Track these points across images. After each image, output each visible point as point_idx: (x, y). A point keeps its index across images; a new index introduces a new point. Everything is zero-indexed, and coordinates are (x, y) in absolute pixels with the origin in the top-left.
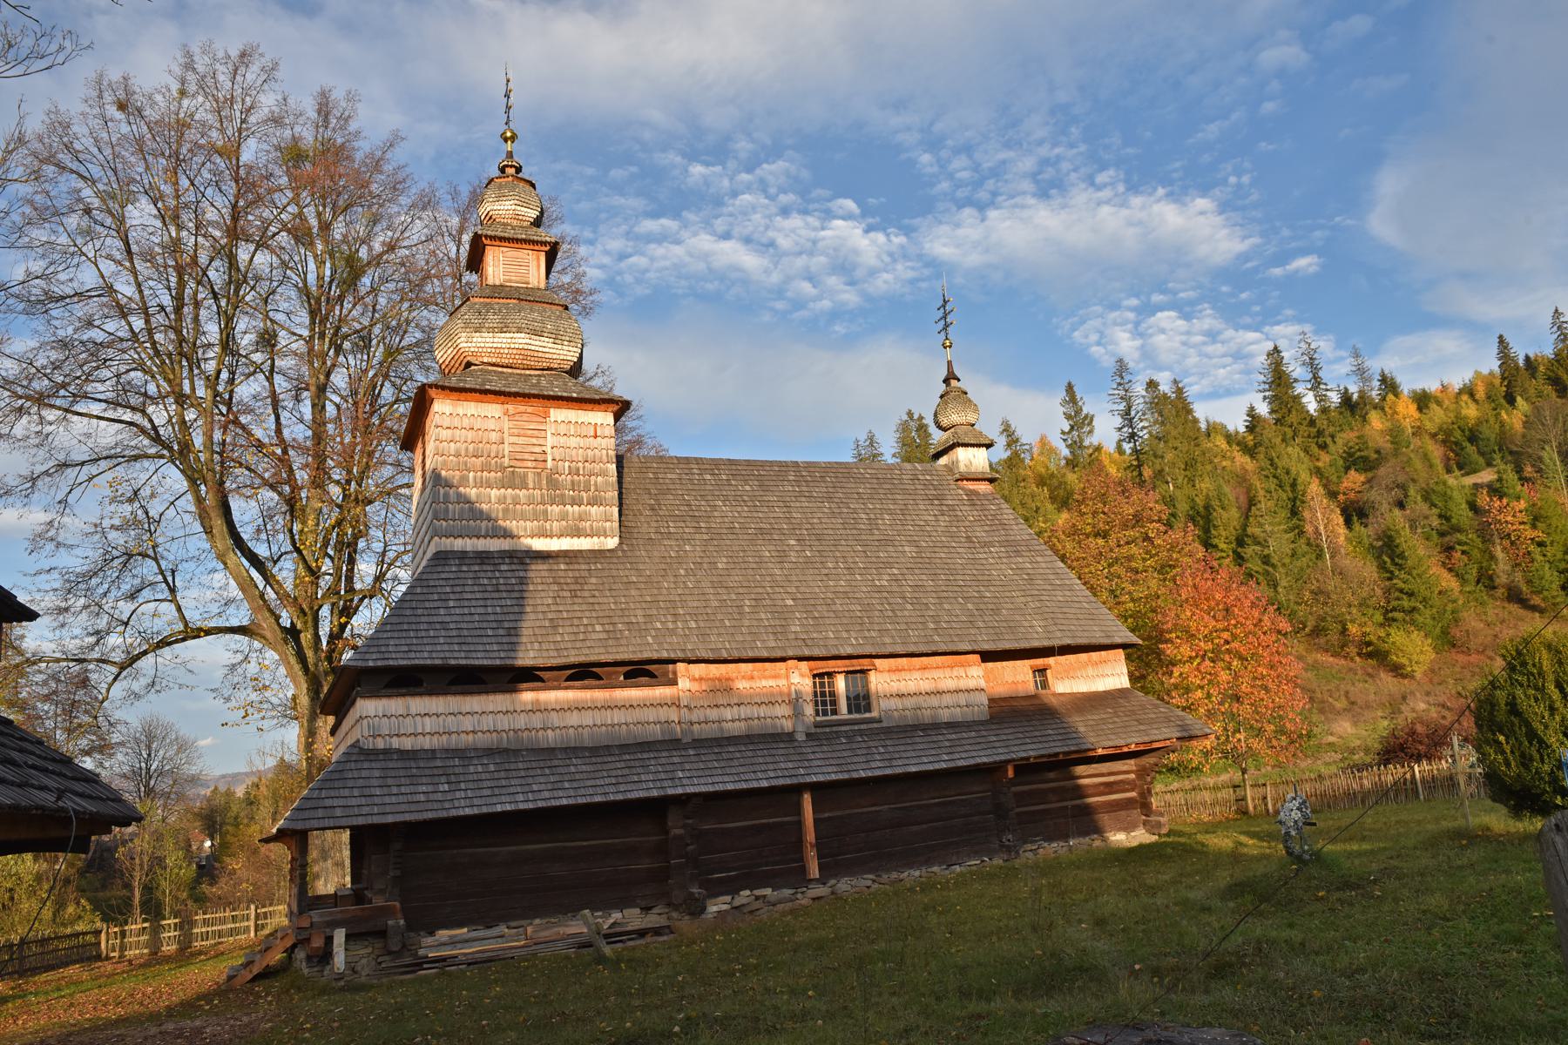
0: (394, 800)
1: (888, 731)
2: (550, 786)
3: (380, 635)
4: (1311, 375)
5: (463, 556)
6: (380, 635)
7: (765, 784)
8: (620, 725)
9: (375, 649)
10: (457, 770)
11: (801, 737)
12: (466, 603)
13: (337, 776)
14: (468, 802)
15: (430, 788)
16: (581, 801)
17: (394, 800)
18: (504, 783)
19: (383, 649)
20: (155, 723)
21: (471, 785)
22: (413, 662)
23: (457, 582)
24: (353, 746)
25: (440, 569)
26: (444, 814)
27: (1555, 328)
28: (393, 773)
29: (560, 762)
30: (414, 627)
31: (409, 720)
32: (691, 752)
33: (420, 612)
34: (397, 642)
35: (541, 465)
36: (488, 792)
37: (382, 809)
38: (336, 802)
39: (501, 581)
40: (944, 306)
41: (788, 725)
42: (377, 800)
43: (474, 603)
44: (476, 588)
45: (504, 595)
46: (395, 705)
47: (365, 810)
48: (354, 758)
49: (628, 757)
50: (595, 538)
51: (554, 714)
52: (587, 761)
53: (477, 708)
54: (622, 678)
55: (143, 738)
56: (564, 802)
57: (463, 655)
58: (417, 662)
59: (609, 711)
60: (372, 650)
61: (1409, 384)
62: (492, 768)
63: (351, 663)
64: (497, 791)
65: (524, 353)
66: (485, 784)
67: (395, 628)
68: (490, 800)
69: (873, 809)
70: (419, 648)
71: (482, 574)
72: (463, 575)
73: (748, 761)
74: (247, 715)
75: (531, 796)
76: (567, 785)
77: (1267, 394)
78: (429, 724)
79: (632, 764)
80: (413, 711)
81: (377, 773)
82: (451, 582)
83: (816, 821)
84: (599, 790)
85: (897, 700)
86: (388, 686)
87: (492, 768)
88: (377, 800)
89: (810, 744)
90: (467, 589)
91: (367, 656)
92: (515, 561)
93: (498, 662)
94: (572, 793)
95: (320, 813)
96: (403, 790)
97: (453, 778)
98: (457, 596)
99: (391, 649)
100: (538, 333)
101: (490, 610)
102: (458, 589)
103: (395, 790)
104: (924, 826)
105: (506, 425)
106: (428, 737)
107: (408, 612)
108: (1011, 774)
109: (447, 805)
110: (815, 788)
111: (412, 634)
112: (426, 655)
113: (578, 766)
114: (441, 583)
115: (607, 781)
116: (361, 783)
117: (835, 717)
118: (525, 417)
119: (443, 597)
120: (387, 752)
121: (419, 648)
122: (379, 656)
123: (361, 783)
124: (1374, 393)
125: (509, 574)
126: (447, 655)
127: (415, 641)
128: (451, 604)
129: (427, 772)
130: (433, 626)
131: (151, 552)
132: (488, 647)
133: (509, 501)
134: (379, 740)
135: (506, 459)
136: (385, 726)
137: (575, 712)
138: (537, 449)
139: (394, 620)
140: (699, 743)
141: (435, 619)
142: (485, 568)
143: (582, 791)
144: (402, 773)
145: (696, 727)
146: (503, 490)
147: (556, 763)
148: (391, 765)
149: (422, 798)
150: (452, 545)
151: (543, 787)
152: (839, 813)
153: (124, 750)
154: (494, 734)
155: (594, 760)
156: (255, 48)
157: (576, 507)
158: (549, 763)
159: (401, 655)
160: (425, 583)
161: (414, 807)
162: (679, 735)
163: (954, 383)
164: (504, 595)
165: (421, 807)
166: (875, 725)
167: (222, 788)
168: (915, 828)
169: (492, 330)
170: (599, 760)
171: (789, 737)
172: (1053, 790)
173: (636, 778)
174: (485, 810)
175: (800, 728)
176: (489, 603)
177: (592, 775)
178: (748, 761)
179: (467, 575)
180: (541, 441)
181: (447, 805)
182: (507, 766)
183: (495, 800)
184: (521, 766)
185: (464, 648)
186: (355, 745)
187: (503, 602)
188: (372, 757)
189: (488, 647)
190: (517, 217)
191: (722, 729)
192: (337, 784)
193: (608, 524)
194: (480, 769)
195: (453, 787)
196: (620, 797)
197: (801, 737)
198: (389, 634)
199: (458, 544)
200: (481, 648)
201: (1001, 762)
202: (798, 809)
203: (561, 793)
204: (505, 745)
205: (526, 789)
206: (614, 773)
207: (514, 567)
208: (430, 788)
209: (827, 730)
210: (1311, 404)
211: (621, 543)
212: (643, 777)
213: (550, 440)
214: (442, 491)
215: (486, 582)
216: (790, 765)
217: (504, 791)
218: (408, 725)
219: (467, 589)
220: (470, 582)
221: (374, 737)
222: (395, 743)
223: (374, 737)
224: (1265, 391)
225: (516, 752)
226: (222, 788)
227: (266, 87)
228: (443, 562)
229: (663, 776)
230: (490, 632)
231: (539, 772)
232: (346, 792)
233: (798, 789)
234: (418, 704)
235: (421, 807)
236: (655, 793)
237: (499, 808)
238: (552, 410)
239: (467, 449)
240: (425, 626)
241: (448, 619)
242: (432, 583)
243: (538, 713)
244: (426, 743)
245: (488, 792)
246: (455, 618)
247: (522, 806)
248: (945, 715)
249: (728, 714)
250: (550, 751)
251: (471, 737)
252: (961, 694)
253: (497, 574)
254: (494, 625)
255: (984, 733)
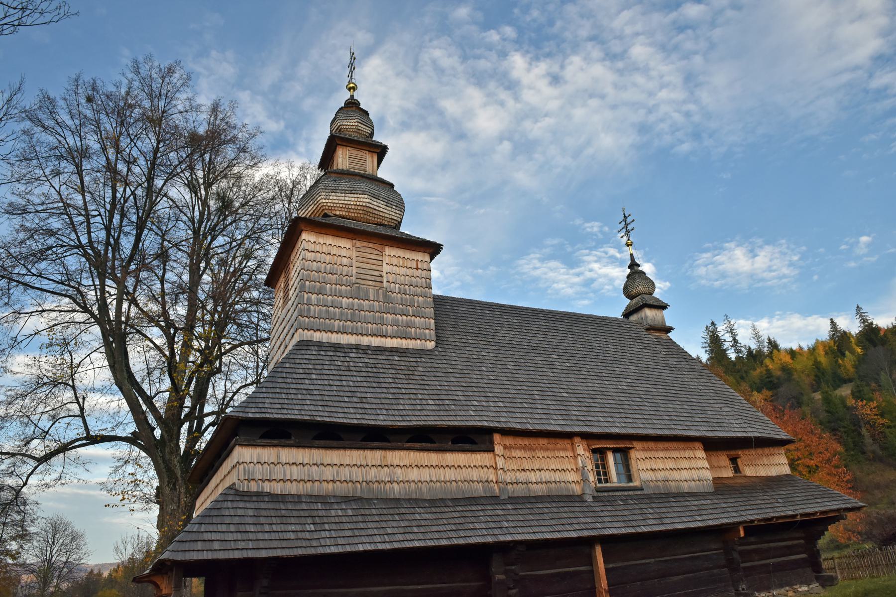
0: (267, 536)
1: (649, 497)
2: (401, 530)
3: (258, 395)
4: (732, 339)
5: (320, 345)
6: (258, 395)
7: (574, 535)
8: (450, 482)
9: (254, 405)
10: (321, 513)
11: (589, 499)
12: (326, 377)
13: (215, 513)
14: (332, 541)
15: (299, 528)
16: (430, 543)
17: (267, 536)
18: (362, 525)
19: (260, 405)
20: (59, 522)
21: (334, 527)
22: (286, 417)
23: (317, 362)
24: (230, 488)
25: (303, 352)
26: (312, 551)
27: (858, 316)
28: (264, 513)
29: (407, 511)
30: (285, 391)
31: (279, 467)
32: (510, 507)
33: (289, 381)
34: (272, 401)
35: (379, 284)
36: (349, 533)
37: (255, 544)
38: (214, 536)
39: (352, 364)
40: (625, 220)
41: (577, 489)
42: (251, 536)
43: (332, 377)
44: (332, 367)
45: (355, 373)
46: (268, 454)
47: (241, 545)
48: (230, 498)
49: (461, 509)
50: (418, 341)
51: (398, 470)
52: (429, 510)
53: (336, 461)
54: (450, 443)
55: (51, 530)
56: (417, 544)
57: (326, 414)
58: (289, 416)
59: (442, 469)
60: (251, 405)
61: (784, 345)
62: (350, 512)
63: (233, 414)
64: (357, 533)
65: (366, 210)
66: (346, 526)
67: (269, 390)
68: (351, 540)
69: (643, 561)
70: (290, 407)
71: (337, 358)
72: (321, 357)
73: (555, 516)
74: (124, 499)
75: (387, 538)
76: (415, 530)
77: (707, 349)
78: (296, 473)
79: (466, 514)
80: (283, 460)
81: (251, 512)
82: (313, 362)
83: (606, 569)
84: (444, 535)
85: (651, 473)
86: (262, 437)
87: (350, 512)
88: (251, 536)
89: (597, 504)
90: (326, 367)
91: (247, 410)
92: (360, 351)
93: (355, 422)
94: (421, 536)
95: (199, 546)
96: (275, 528)
97: (317, 520)
98: (318, 372)
99: (267, 406)
100: (377, 197)
101: (344, 383)
102: (319, 367)
103: (267, 528)
104: (681, 577)
105: (354, 254)
106: (295, 483)
107: (280, 380)
108: (742, 534)
109: (315, 543)
110: (607, 541)
111: (283, 396)
112: (296, 412)
113: (421, 515)
114: (305, 361)
115: (449, 527)
116: (236, 520)
117: (608, 485)
118: (367, 250)
119: (307, 371)
120: (259, 495)
121: (290, 407)
122: (257, 410)
123: (236, 520)
124: (765, 350)
125: (357, 360)
126: (314, 413)
127: (286, 401)
128: (314, 377)
129: (295, 513)
130: (301, 392)
131: (70, 383)
132: (346, 410)
133: (356, 307)
134: (253, 483)
135: (354, 279)
136: (259, 472)
137: (415, 469)
138: (376, 273)
139: (271, 379)
140: (514, 500)
141: (302, 387)
142: (338, 354)
143: (430, 536)
144: (273, 513)
145: (510, 486)
146: (351, 300)
147: (403, 511)
148: (263, 505)
149: (292, 536)
150: (312, 336)
151: (396, 530)
152: (620, 564)
153: (38, 538)
154: (350, 484)
155: (433, 510)
156: (178, 63)
157: (404, 317)
158: (397, 511)
159: (276, 411)
160: (293, 361)
161: (284, 544)
162: (497, 493)
163: (636, 268)
164: (355, 373)
165: (290, 544)
166: (639, 492)
167: (96, 572)
168: (675, 578)
169: (345, 192)
170: (438, 510)
171: (580, 498)
172: (754, 551)
173: (471, 526)
174: (348, 549)
175: (588, 492)
176: (343, 378)
177: (435, 522)
178: (555, 516)
179: (324, 358)
180: (379, 268)
181: (315, 543)
182: (363, 512)
183: (356, 540)
184: (374, 512)
185: (327, 409)
186: (232, 487)
187: (354, 379)
188: (246, 498)
189: (346, 410)
190: (358, 131)
191: (529, 490)
192: (215, 520)
193: (427, 331)
194: (340, 513)
195: (319, 527)
196: (462, 542)
197: (589, 499)
198: (265, 395)
199: (317, 336)
200: (340, 410)
201: (734, 524)
202: (590, 560)
203: (412, 537)
204: (359, 494)
205: (382, 531)
206: (452, 521)
207: (360, 355)
208: (299, 528)
209: (606, 494)
210: (732, 355)
211: (436, 347)
212: (477, 526)
213: (386, 268)
214: (306, 296)
215: (339, 363)
216: (589, 520)
217: (363, 533)
218: (278, 472)
219: (326, 367)
220: (327, 363)
221: (248, 480)
222: (267, 487)
223: (248, 480)
224: (706, 347)
225: (369, 500)
226: (96, 572)
227: (182, 89)
228: (305, 348)
229: (492, 525)
230: (346, 399)
231: (390, 518)
232: (224, 528)
233: (589, 542)
234: (287, 454)
235: (290, 544)
236: (490, 539)
237: (361, 548)
238: (387, 248)
239: (325, 268)
240: (294, 391)
241: (312, 387)
242: (298, 361)
243: (386, 469)
244: (293, 489)
245: (349, 533)
246: (317, 387)
247: (381, 547)
248: (685, 487)
249: (533, 477)
250: (396, 501)
251: (331, 485)
252: (693, 471)
253: (348, 359)
254: (349, 394)
255: (716, 501)
